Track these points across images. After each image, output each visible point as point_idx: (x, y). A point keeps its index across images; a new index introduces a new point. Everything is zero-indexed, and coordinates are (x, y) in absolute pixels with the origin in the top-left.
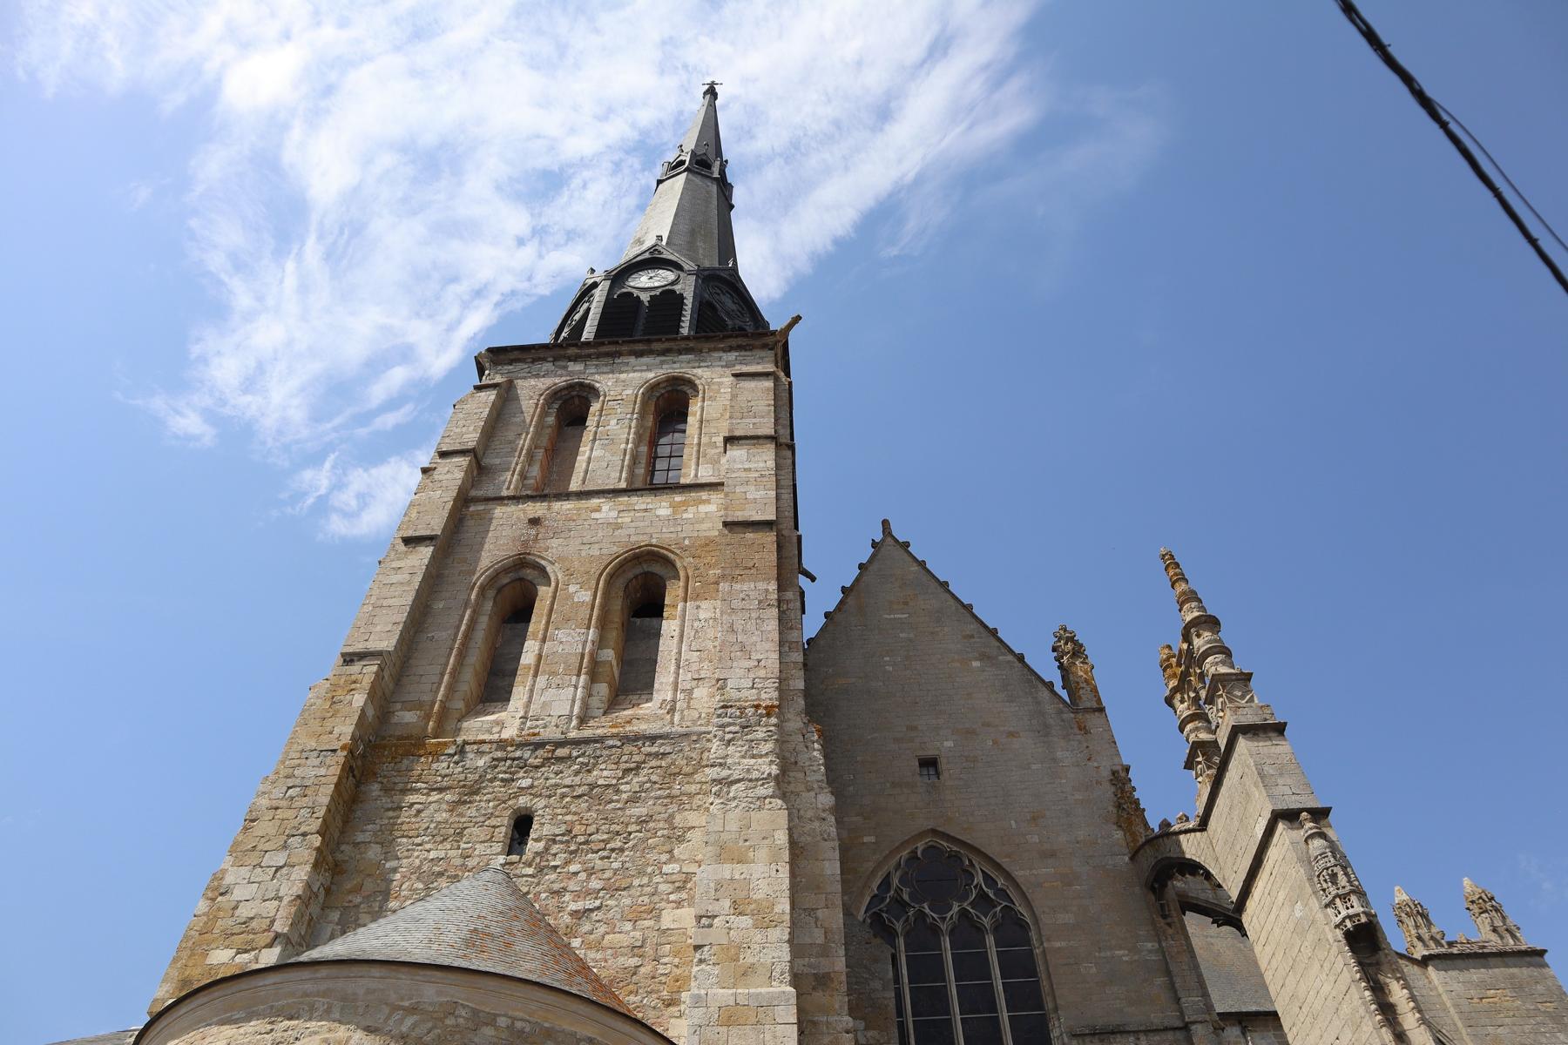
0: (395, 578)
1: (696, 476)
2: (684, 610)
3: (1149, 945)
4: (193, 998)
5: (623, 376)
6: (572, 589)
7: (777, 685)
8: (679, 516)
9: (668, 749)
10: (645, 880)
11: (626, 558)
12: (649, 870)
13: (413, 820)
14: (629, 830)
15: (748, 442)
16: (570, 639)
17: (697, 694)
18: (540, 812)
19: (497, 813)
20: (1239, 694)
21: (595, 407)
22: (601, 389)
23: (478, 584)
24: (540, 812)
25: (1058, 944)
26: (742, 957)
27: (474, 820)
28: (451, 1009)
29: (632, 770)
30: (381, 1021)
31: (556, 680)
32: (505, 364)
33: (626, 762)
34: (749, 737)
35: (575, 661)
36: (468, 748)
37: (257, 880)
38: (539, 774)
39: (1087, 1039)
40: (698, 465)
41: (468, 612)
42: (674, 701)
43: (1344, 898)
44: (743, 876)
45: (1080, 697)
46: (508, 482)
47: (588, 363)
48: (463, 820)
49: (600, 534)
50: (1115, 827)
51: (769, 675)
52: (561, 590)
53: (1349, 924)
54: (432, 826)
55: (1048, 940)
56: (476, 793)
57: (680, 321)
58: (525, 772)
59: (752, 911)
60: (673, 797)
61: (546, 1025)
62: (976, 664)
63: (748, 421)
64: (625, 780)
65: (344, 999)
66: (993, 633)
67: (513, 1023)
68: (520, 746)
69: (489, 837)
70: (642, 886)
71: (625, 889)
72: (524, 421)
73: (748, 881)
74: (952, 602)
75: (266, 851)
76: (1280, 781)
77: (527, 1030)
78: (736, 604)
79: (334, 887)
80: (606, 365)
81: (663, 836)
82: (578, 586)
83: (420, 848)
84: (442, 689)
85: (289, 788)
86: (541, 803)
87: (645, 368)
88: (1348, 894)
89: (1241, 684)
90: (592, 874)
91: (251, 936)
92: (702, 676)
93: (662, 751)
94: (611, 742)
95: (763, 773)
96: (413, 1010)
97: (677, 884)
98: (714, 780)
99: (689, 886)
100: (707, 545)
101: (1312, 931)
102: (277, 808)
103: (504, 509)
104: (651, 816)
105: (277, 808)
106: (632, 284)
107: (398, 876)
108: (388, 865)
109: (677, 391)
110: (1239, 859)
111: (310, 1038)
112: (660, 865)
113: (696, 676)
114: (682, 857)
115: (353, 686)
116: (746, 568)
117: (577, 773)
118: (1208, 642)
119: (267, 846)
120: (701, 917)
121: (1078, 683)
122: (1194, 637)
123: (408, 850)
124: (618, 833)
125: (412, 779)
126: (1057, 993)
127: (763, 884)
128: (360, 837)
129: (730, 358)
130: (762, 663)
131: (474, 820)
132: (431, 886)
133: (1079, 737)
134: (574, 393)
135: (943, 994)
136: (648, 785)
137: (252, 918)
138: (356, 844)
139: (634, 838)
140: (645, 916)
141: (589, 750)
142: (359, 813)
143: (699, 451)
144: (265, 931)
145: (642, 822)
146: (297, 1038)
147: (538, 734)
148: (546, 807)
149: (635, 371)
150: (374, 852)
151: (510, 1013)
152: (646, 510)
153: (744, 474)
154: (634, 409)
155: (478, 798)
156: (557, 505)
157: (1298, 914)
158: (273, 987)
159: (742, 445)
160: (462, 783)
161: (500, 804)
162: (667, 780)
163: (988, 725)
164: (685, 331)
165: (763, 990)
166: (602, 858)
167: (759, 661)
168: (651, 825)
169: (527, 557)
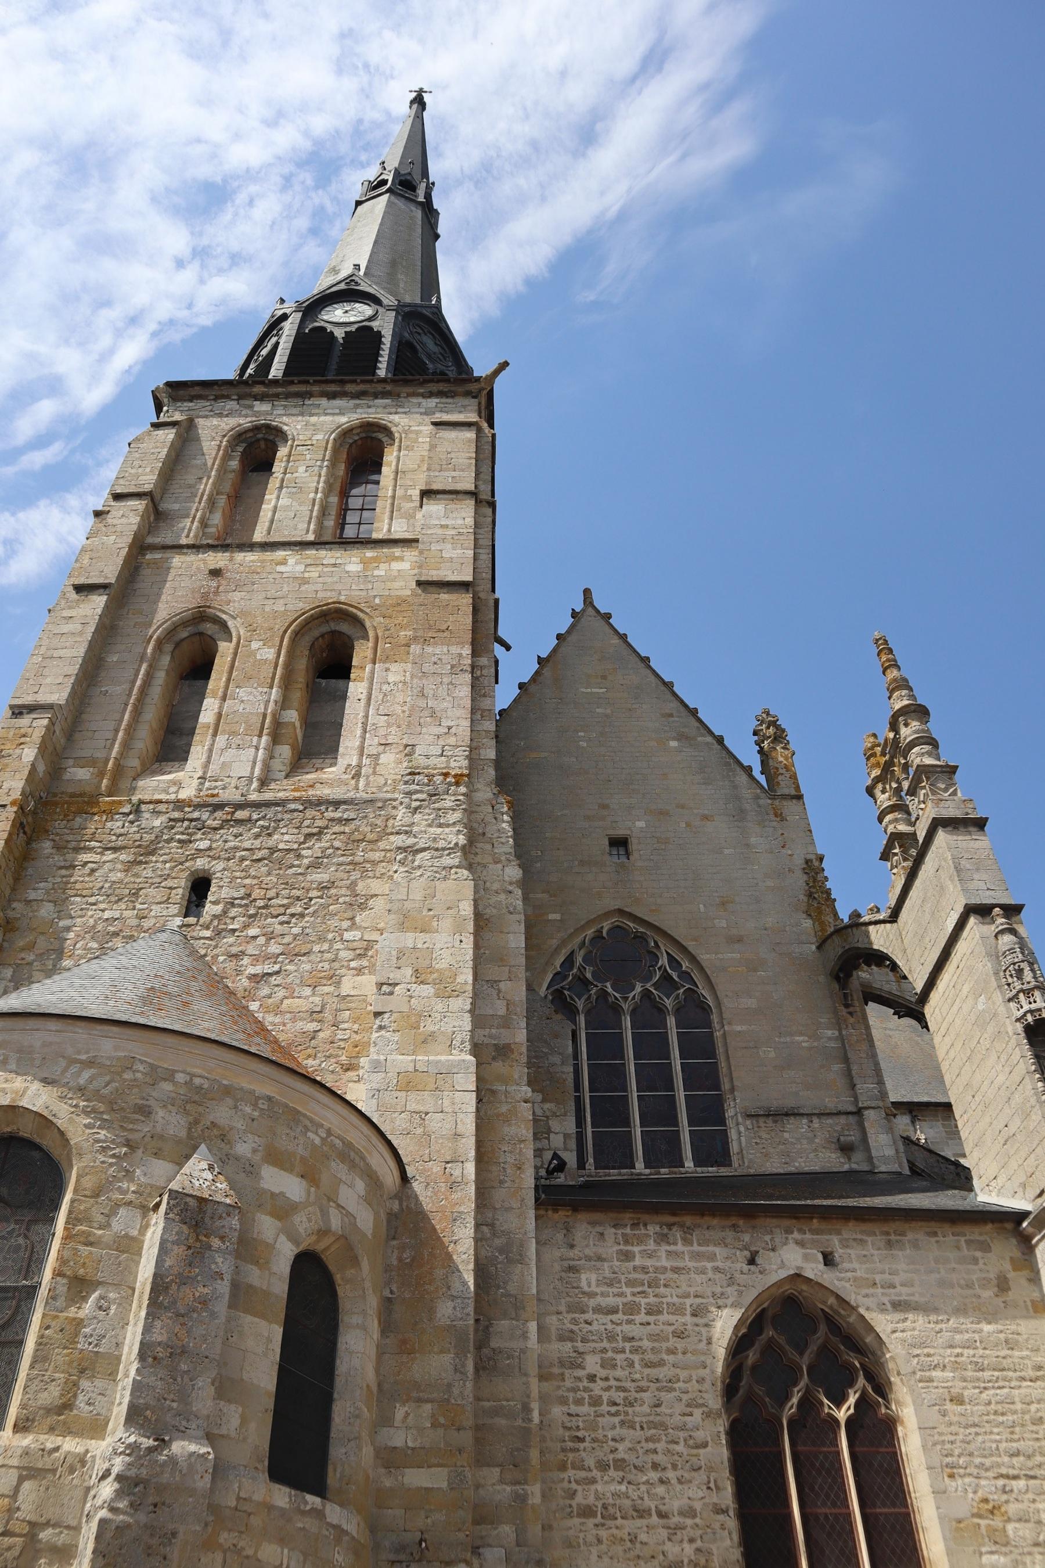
0: (66, 628)
1: (389, 530)
2: (373, 672)
3: (829, 1033)
5: (314, 419)
6: (255, 645)
7: (467, 753)
8: (369, 573)
9: (352, 815)
10: (326, 946)
11: (312, 616)
12: (330, 936)
13: (87, 879)
14: (310, 895)
16: (251, 698)
17: (383, 759)
18: (218, 875)
20: (943, 786)
21: (282, 452)
22: (289, 433)
24: (218, 875)
25: (739, 1028)
26: (422, 1025)
27: (150, 881)
31: (237, 740)
32: (185, 401)
33: (308, 827)
34: (436, 805)
36: (143, 807)
38: (218, 836)
39: (762, 1120)
40: (391, 519)
41: (144, 666)
42: (359, 766)
43: (1028, 993)
44: (425, 946)
46: (187, 530)
48: (138, 880)
50: (804, 916)
51: (459, 743)
53: (1030, 1018)
54: (107, 885)
55: (729, 1024)
56: (152, 853)
57: (377, 361)
58: (203, 834)
61: (225, 1082)
62: (674, 744)
63: (446, 474)
65: (20, 1051)
66: (694, 712)
67: (191, 1079)
68: (199, 806)
71: (304, 954)
72: (205, 464)
74: (652, 678)
76: (976, 876)
77: (206, 1086)
80: (295, 407)
81: (345, 903)
82: (261, 643)
83: (94, 907)
84: (116, 746)
86: (220, 865)
87: (337, 411)
88: (1032, 989)
89: (945, 777)
90: (271, 938)
93: (345, 816)
94: (292, 806)
95: (450, 843)
96: (90, 1063)
97: (358, 952)
99: (370, 953)
101: (993, 1023)
103: (183, 558)
104: (333, 883)
106: (325, 318)
107: (71, 935)
108: (61, 924)
109: (372, 438)
110: (926, 953)
112: (340, 931)
114: (364, 925)
115: (23, 740)
116: (439, 631)
117: (257, 836)
118: (916, 732)
120: (382, 984)
121: (777, 769)
122: (902, 727)
123: (82, 909)
124: (298, 899)
125: (86, 837)
126: (734, 1075)
127: (446, 953)
128: (32, 895)
130: (453, 730)
131: (150, 881)
132: (106, 946)
133: (775, 823)
134: (260, 436)
135: (620, 1072)
136: (331, 851)
138: (28, 902)
140: (325, 982)
141: (270, 813)
143: (393, 504)
145: (323, 888)
147: (217, 795)
148: (224, 869)
149: (326, 414)
150: (46, 911)
151: (189, 1070)
152: (334, 565)
153: (440, 531)
154: (324, 456)
155: (154, 859)
157: (981, 1007)
159: (440, 499)
162: (350, 847)
163: (683, 807)
165: (443, 1058)
166: (282, 923)
167: (449, 728)
168: (333, 891)
169: (208, 610)
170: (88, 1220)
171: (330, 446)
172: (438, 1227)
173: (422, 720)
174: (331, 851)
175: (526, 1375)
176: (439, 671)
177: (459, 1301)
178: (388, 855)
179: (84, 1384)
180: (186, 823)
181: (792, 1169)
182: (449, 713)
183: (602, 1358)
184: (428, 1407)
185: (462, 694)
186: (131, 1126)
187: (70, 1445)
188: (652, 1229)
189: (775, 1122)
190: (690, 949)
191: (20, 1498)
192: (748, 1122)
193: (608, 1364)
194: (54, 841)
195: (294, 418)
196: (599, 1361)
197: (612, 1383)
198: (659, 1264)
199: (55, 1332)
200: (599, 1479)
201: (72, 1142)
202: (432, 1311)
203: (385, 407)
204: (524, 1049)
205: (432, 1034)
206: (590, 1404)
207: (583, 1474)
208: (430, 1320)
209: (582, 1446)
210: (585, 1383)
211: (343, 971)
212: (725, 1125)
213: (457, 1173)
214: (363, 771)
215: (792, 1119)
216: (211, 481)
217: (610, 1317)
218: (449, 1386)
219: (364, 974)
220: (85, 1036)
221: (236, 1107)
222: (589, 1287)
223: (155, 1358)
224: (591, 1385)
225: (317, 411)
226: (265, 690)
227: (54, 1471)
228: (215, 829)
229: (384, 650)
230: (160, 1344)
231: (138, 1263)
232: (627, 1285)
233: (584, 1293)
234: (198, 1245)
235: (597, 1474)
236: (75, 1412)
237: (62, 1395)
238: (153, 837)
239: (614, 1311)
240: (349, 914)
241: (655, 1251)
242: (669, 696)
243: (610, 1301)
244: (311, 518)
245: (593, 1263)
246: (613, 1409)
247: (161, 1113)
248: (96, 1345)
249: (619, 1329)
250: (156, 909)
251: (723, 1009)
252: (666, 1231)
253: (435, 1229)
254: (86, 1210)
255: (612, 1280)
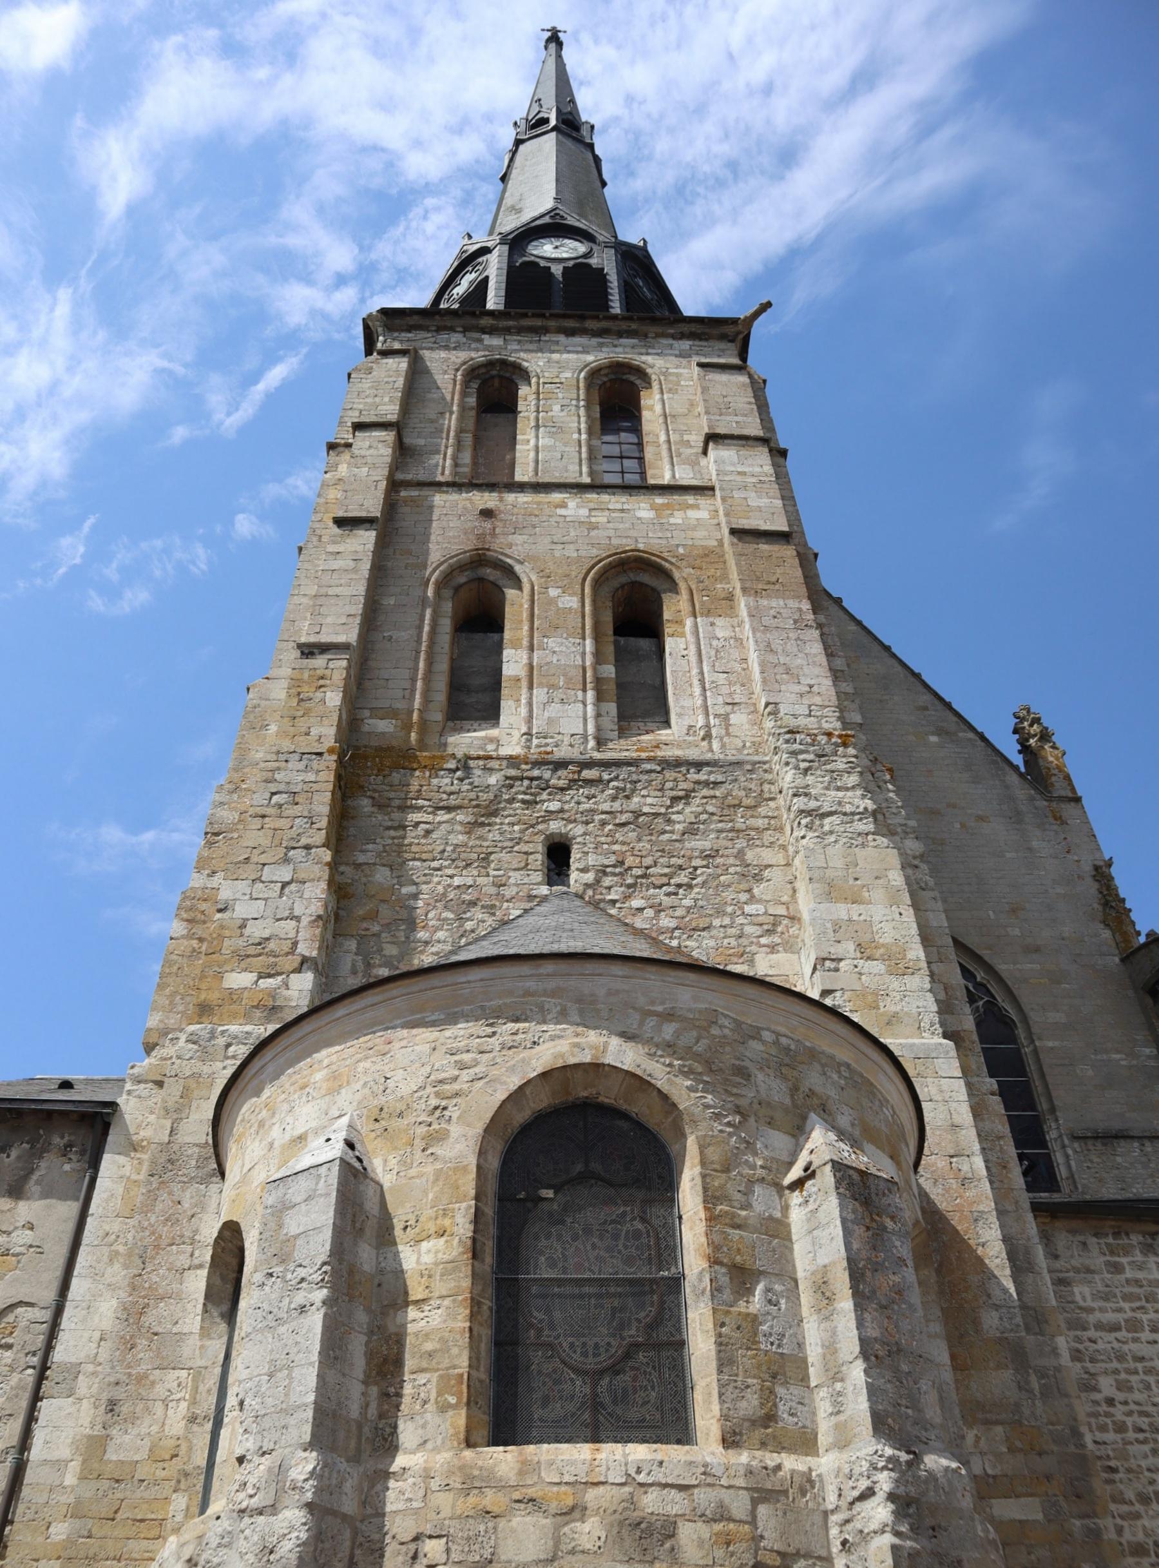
0: (336, 564)
1: (674, 476)
2: (696, 625)
3: (1147, 1051)
4: (357, 998)
5: (556, 356)
6: (553, 592)
7: (837, 714)
9: (720, 778)
11: (610, 563)
12: (729, 909)
13: (423, 841)
14: (693, 864)
15: (735, 442)
17: (734, 719)
18: (579, 840)
19: (526, 838)
21: (523, 391)
22: (530, 369)
23: (433, 580)
24: (579, 840)
25: (1050, 1044)
26: (882, 1004)
27: (500, 845)
28: (712, 1018)
29: (680, 798)
30: (635, 1026)
31: (559, 694)
32: (402, 331)
33: (672, 789)
34: (828, 767)
35: (577, 674)
36: (472, 763)
37: (261, 896)
38: (568, 798)
39: (1090, 1142)
40: (672, 464)
41: (428, 613)
42: (707, 726)
44: (862, 918)
45: (1052, 785)
46: (443, 466)
47: (507, 337)
48: (485, 844)
49: (573, 534)
50: (1102, 926)
51: (827, 703)
52: (539, 593)
54: (449, 849)
55: (1040, 1039)
56: (495, 813)
57: (607, 300)
58: (550, 794)
59: (882, 955)
60: (738, 831)
61: (808, 1044)
62: (934, 739)
63: (728, 418)
64: (675, 809)
65: (579, 1000)
68: (537, 764)
69: (523, 864)
70: (725, 927)
71: (704, 929)
72: (444, 398)
73: (869, 923)
74: (899, 668)
75: (264, 865)
77: (793, 1047)
78: (766, 621)
79: (342, 913)
80: (531, 342)
81: (736, 873)
82: (560, 590)
83: (439, 873)
84: (418, 696)
85: (273, 794)
86: (579, 830)
87: (580, 349)
90: (660, 911)
91: (272, 959)
92: (736, 701)
93: (712, 779)
94: (648, 766)
95: (858, 807)
96: (669, 1016)
97: (766, 927)
98: (802, 811)
99: (779, 929)
100: (706, 555)
102: (263, 816)
103: (445, 497)
104: (717, 851)
105: (263, 816)
106: (535, 252)
107: (420, 903)
108: (404, 890)
109: (623, 381)
111: (552, 1043)
112: (739, 905)
113: (729, 701)
114: (764, 897)
115: (321, 682)
116: (769, 583)
117: (614, 798)
119: (263, 859)
120: (824, 959)
123: (425, 875)
124: (681, 868)
125: (411, 795)
126: (1054, 1094)
127: (887, 927)
128: (361, 858)
129: (683, 347)
130: (815, 689)
131: (500, 845)
133: (1055, 827)
134: (494, 372)
136: (705, 816)
137: (268, 939)
138: (358, 866)
139: (702, 874)
140: (735, 960)
141: (624, 772)
142: (352, 831)
143: (670, 449)
144: (287, 954)
145: (709, 856)
146: (534, 1043)
148: (585, 834)
149: (569, 352)
150: (382, 876)
151: (773, 1027)
152: (622, 511)
153: (739, 478)
154: (578, 395)
155: (498, 820)
156: (510, 497)
158: (478, 984)
159: (729, 445)
160: (474, 803)
161: (527, 829)
162: (726, 812)
163: (954, 806)
164: (616, 308)
165: (916, 1041)
166: (668, 894)
167: (811, 687)
168: (719, 860)
169: (488, 553)
170: (725, 1198)
171: (582, 385)
172: (959, 1228)
173: (778, 677)
174: (705, 816)
175: (1067, 1396)
176: (781, 625)
177: (1004, 1310)
178: (772, 822)
179: (780, 1391)
180: (526, 783)
181: (1129, 1196)
182: (806, 670)
183: (1116, 1380)
184: (999, 1429)
185: (814, 651)
186: (735, 1091)
187: (791, 1463)
188: (1135, 1239)
189: (1104, 1144)
190: (986, 958)
191: (760, 1524)
192: (1076, 1145)
193: (1122, 1386)
194: (373, 798)
195: (534, 355)
196: (1114, 1384)
197: (1133, 1407)
198: (1151, 1277)
199: (732, 1330)
200: (1143, 1514)
201: (681, 1107)
202: (976, 1322)
203: (633, 347)
204: (975, 1037)
205: (895, 1015)
206: (1116, 1431)
207: (1125, 1508)
208: (977, 1331)
209: (1117, 1477)
210: (1104, 1408)
211: (754, 948)
212: (1047, 1148)
213: (965, 1168)
214: (714, 732)
215: (1122, 1142)
216: (454, 417)
217: (1114, 1335)
218: (1017, 1405)
219: (778, 952)
220: (658, 983)
221: (825, 1074)
222: (1085, 1301)
223: (876, 1357)
224: (1111, 1410)
225: (556, 348)
226: (578, 641)
227: (785, 1493)
228: (562, 789)
229: (703, 603)
230: (876, 1339)
231: (791, 1250)
232: (1124, 1299)
233: (1080, 1308)
234: (874, 1225)
235: (1138, 1507)
236: (781, 1424)
237: (762, 1404)
238: (491, 796)
239: (1116, 1328)
240: (744, 886)
241: (1144, 1263)
242: (921, 688)
243: (1110, 1317)
244: (581, 460)
245: (1083, 1275)
246: (1141, 1436)
247: (760, 1077)
248: (779, 1346)
249: (1126, 1348)
250: (515, 877)
251: (1031, 1023)
252: (1149, 1241)
253: (957, 1231)
254: (722, 1187)
255: (1107, 1294)
